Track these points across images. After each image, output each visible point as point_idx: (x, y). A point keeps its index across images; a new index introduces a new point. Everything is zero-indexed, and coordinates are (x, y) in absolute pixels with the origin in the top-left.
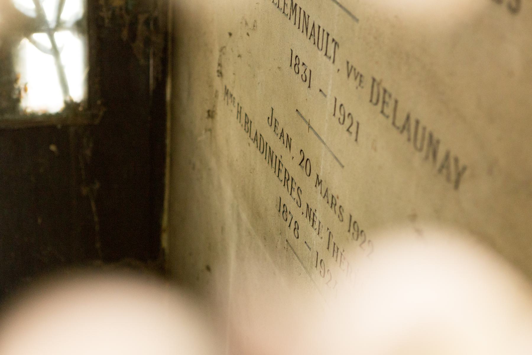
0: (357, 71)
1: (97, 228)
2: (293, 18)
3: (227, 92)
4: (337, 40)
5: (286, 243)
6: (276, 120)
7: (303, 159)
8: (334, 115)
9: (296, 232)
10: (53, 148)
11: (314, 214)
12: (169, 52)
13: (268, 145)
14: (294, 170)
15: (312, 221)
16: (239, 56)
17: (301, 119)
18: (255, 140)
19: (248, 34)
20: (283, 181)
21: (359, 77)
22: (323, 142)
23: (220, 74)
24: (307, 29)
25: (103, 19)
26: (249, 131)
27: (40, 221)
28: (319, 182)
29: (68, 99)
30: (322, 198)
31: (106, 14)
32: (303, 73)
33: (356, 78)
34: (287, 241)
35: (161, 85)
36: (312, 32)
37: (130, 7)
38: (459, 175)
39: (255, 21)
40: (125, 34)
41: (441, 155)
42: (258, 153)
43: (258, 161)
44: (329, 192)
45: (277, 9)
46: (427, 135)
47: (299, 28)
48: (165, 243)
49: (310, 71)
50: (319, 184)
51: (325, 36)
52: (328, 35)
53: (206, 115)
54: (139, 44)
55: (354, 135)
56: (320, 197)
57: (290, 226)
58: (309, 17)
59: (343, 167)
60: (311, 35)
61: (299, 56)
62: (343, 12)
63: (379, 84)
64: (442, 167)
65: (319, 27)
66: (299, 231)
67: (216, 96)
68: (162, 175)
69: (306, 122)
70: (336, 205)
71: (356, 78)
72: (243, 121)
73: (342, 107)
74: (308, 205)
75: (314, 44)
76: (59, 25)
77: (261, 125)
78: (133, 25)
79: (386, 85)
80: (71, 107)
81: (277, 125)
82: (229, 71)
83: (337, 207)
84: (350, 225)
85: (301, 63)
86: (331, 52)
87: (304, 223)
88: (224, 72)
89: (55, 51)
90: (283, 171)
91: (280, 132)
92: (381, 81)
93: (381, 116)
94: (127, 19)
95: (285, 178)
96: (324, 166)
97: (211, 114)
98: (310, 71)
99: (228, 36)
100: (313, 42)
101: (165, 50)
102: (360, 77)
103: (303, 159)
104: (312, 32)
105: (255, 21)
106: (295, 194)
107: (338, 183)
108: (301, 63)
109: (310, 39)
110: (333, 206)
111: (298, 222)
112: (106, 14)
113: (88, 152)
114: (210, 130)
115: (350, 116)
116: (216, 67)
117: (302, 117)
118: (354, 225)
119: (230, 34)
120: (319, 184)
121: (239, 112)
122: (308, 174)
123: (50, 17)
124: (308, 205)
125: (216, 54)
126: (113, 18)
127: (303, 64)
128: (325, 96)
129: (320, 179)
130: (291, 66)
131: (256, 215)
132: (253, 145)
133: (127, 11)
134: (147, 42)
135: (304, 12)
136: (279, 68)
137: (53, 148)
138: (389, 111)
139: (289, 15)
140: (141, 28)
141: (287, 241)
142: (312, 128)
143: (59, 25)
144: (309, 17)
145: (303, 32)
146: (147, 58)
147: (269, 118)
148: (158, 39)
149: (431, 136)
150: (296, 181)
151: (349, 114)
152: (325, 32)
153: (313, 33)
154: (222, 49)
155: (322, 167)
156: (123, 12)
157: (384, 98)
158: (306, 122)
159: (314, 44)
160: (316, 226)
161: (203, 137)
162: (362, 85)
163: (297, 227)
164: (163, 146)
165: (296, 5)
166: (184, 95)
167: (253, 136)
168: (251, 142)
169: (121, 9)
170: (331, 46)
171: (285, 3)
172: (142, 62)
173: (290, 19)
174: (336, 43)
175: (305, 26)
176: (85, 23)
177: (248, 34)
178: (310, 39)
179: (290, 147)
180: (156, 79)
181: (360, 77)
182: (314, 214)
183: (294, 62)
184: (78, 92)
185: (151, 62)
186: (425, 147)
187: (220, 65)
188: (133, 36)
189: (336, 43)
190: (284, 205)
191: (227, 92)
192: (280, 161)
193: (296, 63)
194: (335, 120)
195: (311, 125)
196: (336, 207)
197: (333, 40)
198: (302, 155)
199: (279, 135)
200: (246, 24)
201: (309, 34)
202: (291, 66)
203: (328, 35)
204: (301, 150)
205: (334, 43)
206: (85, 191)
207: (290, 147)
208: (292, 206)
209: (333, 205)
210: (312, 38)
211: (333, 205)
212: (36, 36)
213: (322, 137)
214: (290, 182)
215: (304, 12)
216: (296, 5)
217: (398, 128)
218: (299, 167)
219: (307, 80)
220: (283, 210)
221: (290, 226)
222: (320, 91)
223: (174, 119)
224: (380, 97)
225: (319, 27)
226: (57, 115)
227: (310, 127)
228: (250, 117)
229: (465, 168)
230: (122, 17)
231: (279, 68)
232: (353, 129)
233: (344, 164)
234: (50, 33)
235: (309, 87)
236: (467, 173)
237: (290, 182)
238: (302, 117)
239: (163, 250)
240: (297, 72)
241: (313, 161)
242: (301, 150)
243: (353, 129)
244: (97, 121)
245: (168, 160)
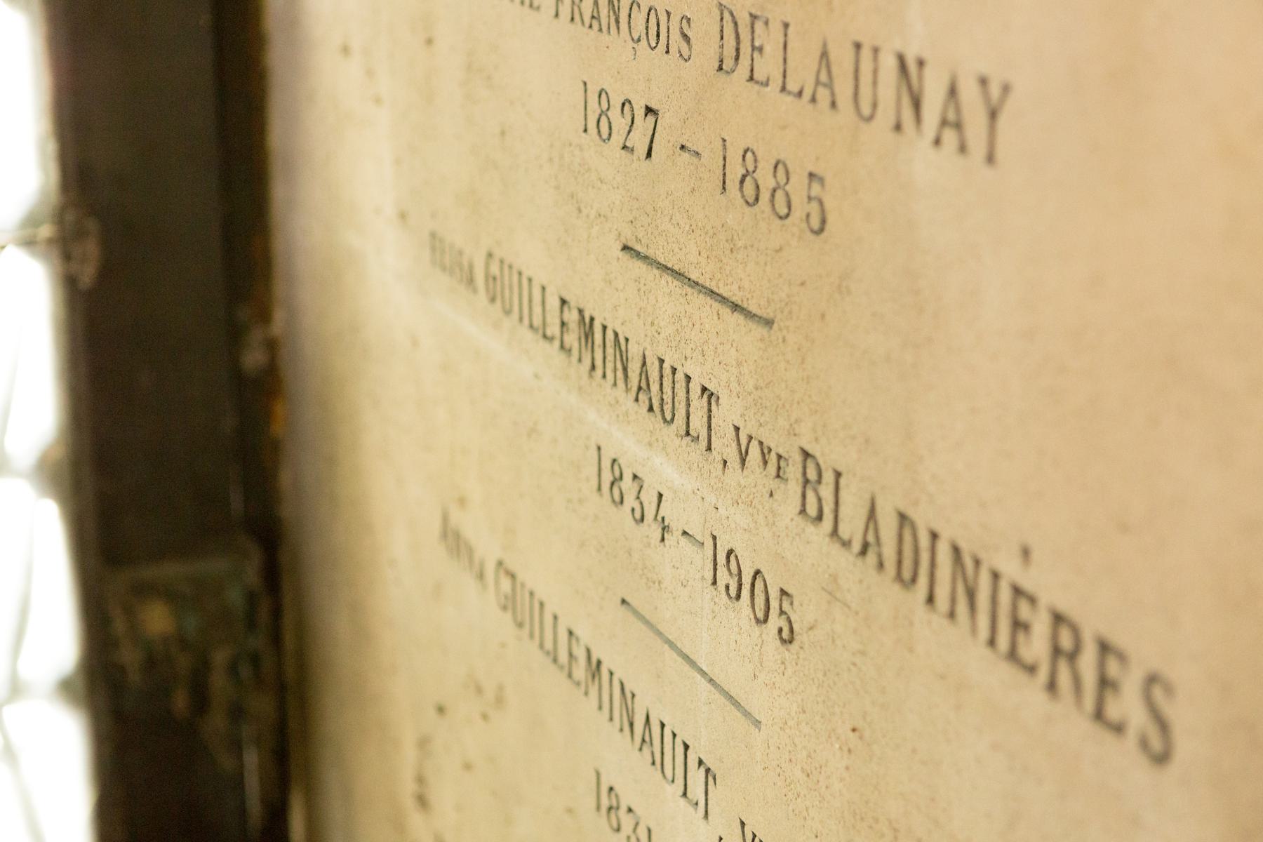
4: (708, 762)
9: (617, 474)
23: (422, 801)
24: (631, 725)
25: (122, 669)
31: (130, 657)
35: (277, 815)
36: (650, 736)
40: (180, 701)
47: (611, 719)
49: (649, 831)
51: (680, 749)
52: (686, 747)
54: (216, 722)
58: (633, 695)
60: (643, 740)
61: (617, 788)
62: (722, 700)
65: (663, 725)
75: (653, 763)
78: (201, 671)
82: (444, 794)
85: (623, 809)
86: (697, 791)
94: (184, 663)
98: (649, 831)
100: (650, 761)
104: (650, 736)
108: (623, 809)
109: (641, 749)
111: (621, 461)
112: (130, 657)
116: (408, 787)
119: (441, 710)
125: (408, 755)
126: (150, 663)
127: (630, 810)
133: (183, 643)
134: (237, 713)
135: (622, 685)
139: (583, 685)
140: (219, 682)
144: (633, 695)
145: (621, 730)
146: (236, 747)
148: (262, 705)
152: (678, 740)
153: (647, 738)
154: (424, 743)
159: (653, 763)
172: (226, 762)
174: (708, 771)
175: (619, 366)
178: (641, 749)
183: (605, 802)
187: (420, 780)
188: (201, 700)
189: (708, 771)
201: (638, 739)
203: (686, 747)
205: (702, 770)
210: (646, 749)
215: (622, 685)
225: (663, 725)
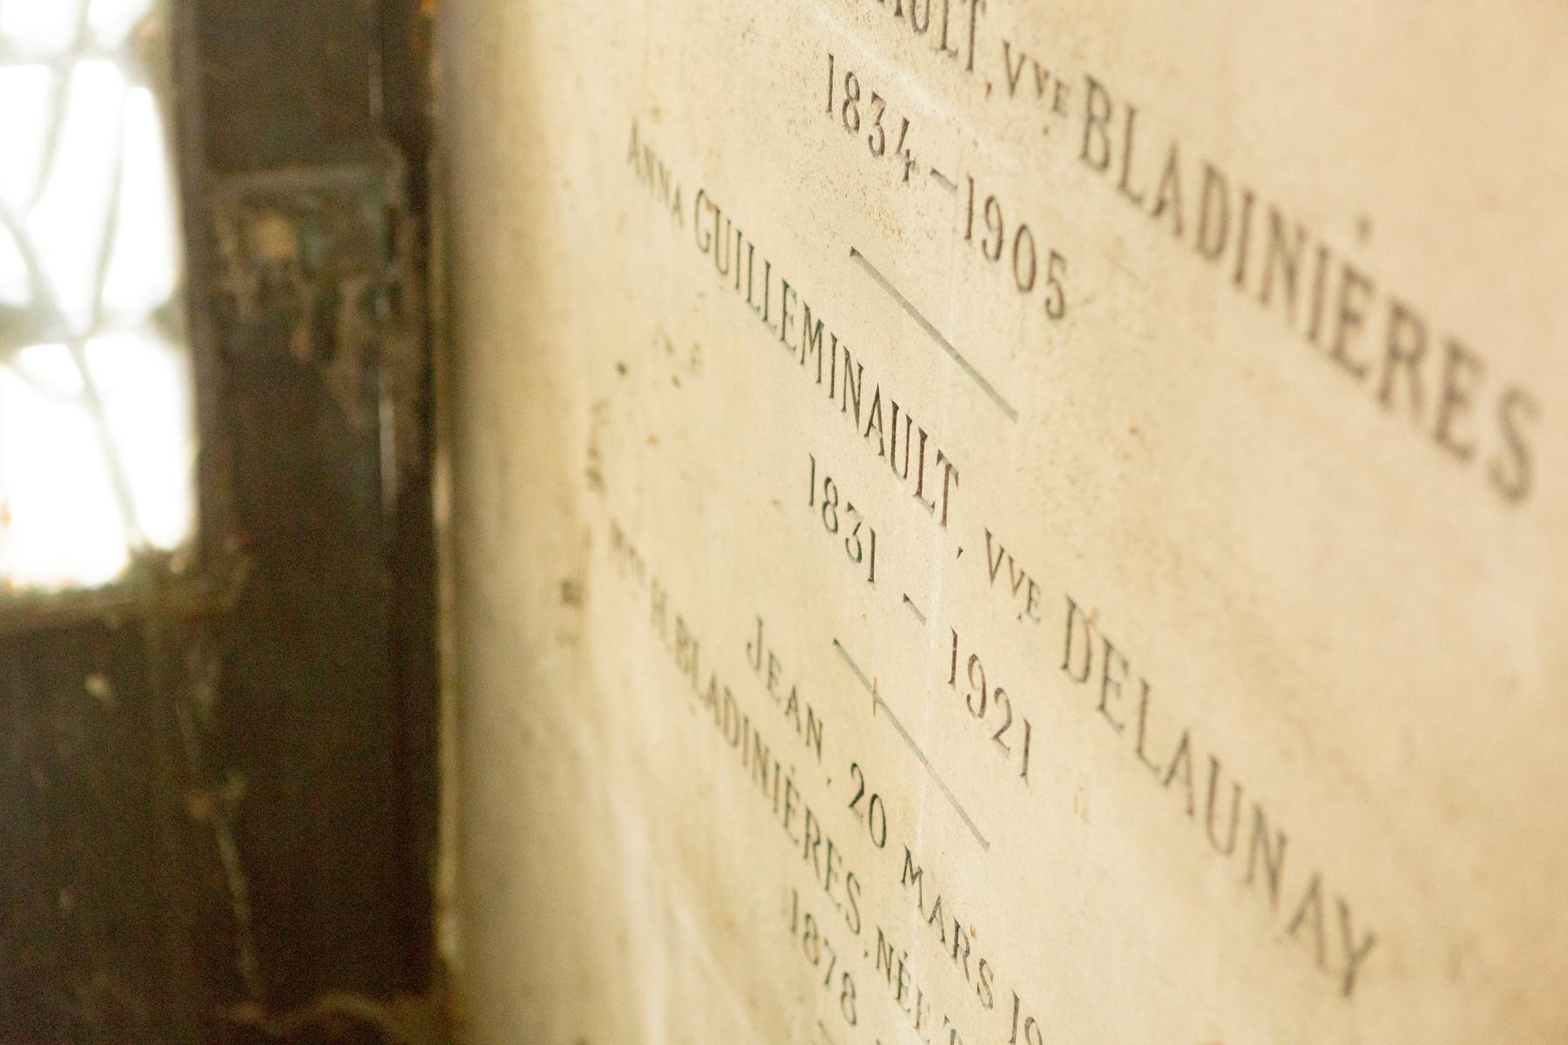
0: (1016, 566)
1: (242, 911)
2: (811, 360)
3: (618, 538)
4: (950, 457)
5: (818, 1030)
6: (772, 656)
7: (861, 793)
8: (952, 681)
10: (97, 686)
11: (901, 965)
12: (439, 379)
13: (751, 725)
14: (837, 821)
15: (895, 984)
16: (653, 440)
17: (850, 669)
18: (711, 699)
19: (676, 381)
20: (802, 842)
21: (1025, 583)
22: (920, 754)
23: (595, 478)
24: (857, 404)
25: (231, 299)
26: (690, 668)
27: (65, 901)
28: (913, 874)
29: (138, 543)
30: (924, 923)
31: (240, 283)
32: (850, 536)
33: (1016, 588)
34: (821, 1025)
35: (418, 483)
36: (880, 419)
37: (315, 260)
38: (1355, 958)
39: (697, 347)
40: (302, 342)
41: (1294, 881)
42: (723, 743)
43: (725, 770)
44: (945, 908)
45: (763, 326)
46: (1247, 813)
48: (449, 939)
50: (913, 878)
52: (924, 437)
53: (557, 594)
54: (344, 370)
55: (1017, 755)
56: (918, 920)
57: (827, 982)
58: (861, 369)
59: (986, 845)
60: (871, 424)
63: (1088, 623)
64: (1299, 918)
66: (858, 1003)
67: (587, 542)
68: (432, 745)
69: (865, 682)
70: (968, 952)
71: (1016, 588)
72: (672, 637)
73: (976, 664)
74: (881, 935)
75: (882, 453)
76: (100, 319)
77: (725, 659)
79: (1111, 627)
80: (151, 565)
81: (775, 670)
83: (973, 961)
84: (1015, 1025)
85: (843, 505)
87: (872, 984)
88: (606, 474)
89: (91, 396)
90: (801, 814)
91: (788, 693)
92: (1095, 613)
93: (1099, 716)
94: (307, 293)
95: (808, 836)
96: (925, 827)
97: (572, 594)
99: (612, 372)
101: (426, 377)
102: (1025, 586)
103: (861, 793)
104: (880, 419)
105: (697, 347)
106: (839, 889)
107: (968, 887)
108: (843, 505)
110: (960, 955)
112: (240, 283)
113: (205, 694)
114: (571, 639)
115: (1001, 696)
116: (579, 463)
117: (852, 665)
118: (1027, 1028)
119: (622, 369)
120: (913, 878)
121: (659, 607)
122: (879, 840)
123: (72, 301)
124: (881, 935)
125: (581, 419)
126: (265, 292)
128: (923, 620)
129: (915, 865)
130: (812, 503)
131: (724, 927)
132: (706, 716)
133: (308, 272)
134: (371, 358)
136: (776, 503)
137: (97, 686)
138: (1124, 707)
140: (349, 320)
141: (821, 1025)
142: (883, 705)
143: (100, 319)
144: (861, 369)
145: (844, 409)
146: (370, 398)
147: (749, 645)
148: (402, 349)
149: (1259, 816)
150: (842, 853)
151: (999, 692)
153: (876, 422)
154: (598, 408)
155: (920, 831)
156: (295, 278)
157: (1106, 668)
158: (865, 682)
159: (882, 453)
160: (910, 999)
161: (551, 661)
162: (1034, 612)
163: (849, 990)
164: (432, 657)
165: (820, 325)
166: (488, 514)
167: (704, 687)
168: (700, 705)
169: (286, 265)
170: (934, 474)
171: (785, 313)
172: (357, 418)
173: (802, 362)
176: (179, 315)
177: (676, 381)
179: (819, 746)
180: (404, 468)
181: (1025, 586)
182: (901, 965)
184: (167, 515)
185: (387, 413)
186: (1243, 846)
187: (593, 453)
188: (327, 342)
190: (808, 917)
191: (618, 538)
192: (789, 783)
193: (826, 498)
194: (956, 698)
195: (881, 694)
196: (969, 960)
197: (940, 457)
198: (858, 780)
199: (784, 704)
200: (670, 348)
201: (864, 422)
202: (812, 503)
203: (924, 437)
204: (855, 765)
205: (942, 465)
206: (199, 806)
207: (819, 746)
208: (830, 924)
209: (959, 950)
211: (959, 950)
212: (31, 356)
213: (920, 744)
214: (822, 850)
216: (820, 325)
217: (1156, 770)
218: (850, 812)
219: (866, 554)
220: (803, 927)
221: (827, 982)
222: (906, 599)
223: (463, 584)
224: (1094, 662)
225: (896, 408)
226: (108, 591)
227: (877, 701)
228: (693, 629)
229: (1370, 941)
230: (288, 288)
231: (776, 503)
232: (1014, 737)
233: (987, 839)
234: (75, 343)
235: (871, 580)
236: (1377, 960)
237: (822, 850)
238: (852, 665)
239: (443, 964)
240: (832, 526)
241: (891, 803)
242: (855, 765)
243: (1014, 737)
244: (227, 601)
245: (448, 702)
